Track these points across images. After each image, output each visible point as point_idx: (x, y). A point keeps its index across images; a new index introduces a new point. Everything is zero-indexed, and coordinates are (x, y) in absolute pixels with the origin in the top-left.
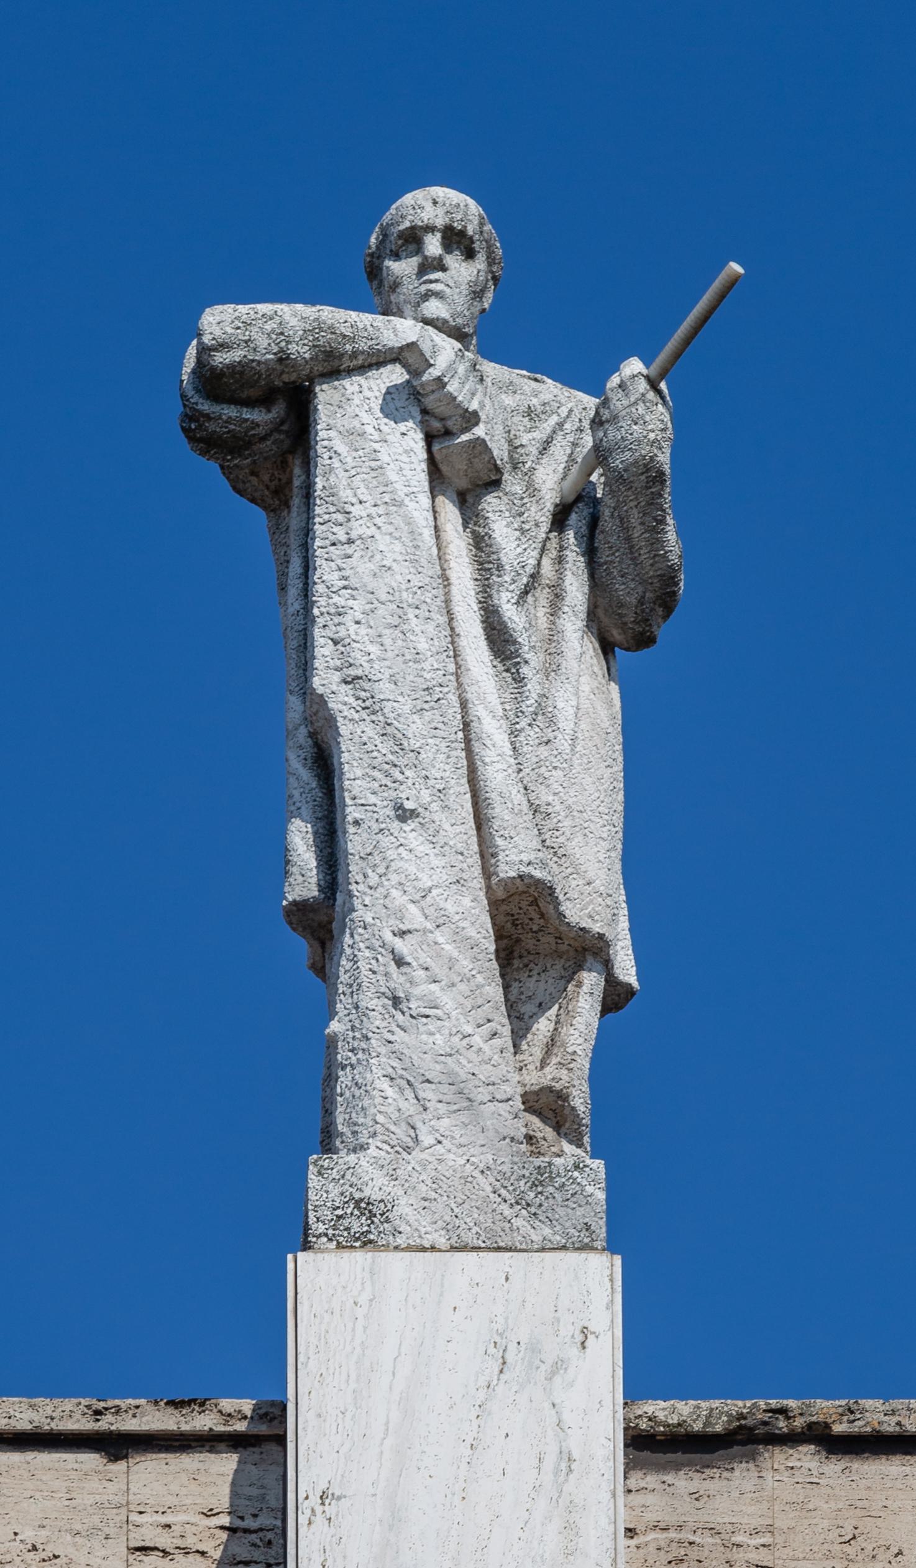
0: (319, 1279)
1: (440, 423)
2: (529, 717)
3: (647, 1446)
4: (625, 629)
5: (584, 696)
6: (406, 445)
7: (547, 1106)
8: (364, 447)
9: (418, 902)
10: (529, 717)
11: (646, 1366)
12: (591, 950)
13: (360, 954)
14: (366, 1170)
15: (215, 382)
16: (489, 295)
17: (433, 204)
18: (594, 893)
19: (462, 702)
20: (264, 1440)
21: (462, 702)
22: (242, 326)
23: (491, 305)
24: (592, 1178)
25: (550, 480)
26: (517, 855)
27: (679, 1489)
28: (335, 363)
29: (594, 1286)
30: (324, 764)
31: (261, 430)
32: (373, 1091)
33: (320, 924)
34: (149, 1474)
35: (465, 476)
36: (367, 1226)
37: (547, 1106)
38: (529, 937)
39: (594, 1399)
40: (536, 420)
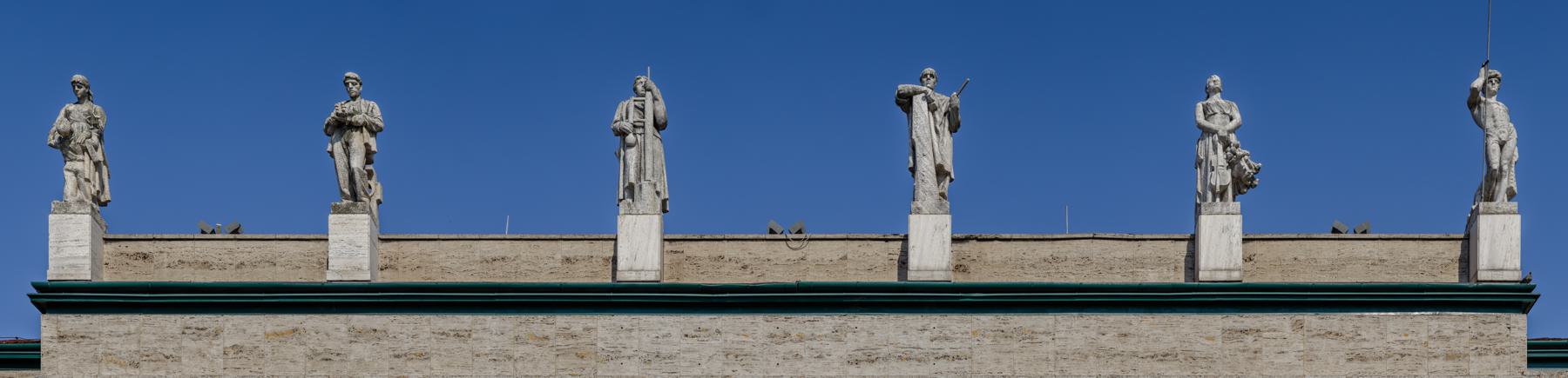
0: (913, 218)
1: (929, 101)
2: (941, 142)
3: (955, 240)
4: (953, 129)
5: (947, 139)
6: (925, 105)
7: (942, 195)
8: (919, 104)
9: (926, 166)
10: (941, 142)
11: (955, 226)
12: (948, 174)
13: (918, 174)
14: (919, 204)
15: (900, 95)
16: (1200, 118)
17: (929, 70)
18: (949, 166)
19: (931, 139)
20: (905, 239)
21: (931, 139)
22: (904, 87)
23: (384, 193)
24: (947, 204)
25: (944, 109)
26: (939, 161)
27: (958, 246)
28: (916, 93)
29: (947, 219)
30: (914, 149)
31: (905, 102)
32: (920, 193)
33: (913, 170)
34: (891, 244)
35: (933, 109)
36: (919, 211)
37: (942, 195)
38: (940, 172)
39: (947, 234)
40: (942, 101)
